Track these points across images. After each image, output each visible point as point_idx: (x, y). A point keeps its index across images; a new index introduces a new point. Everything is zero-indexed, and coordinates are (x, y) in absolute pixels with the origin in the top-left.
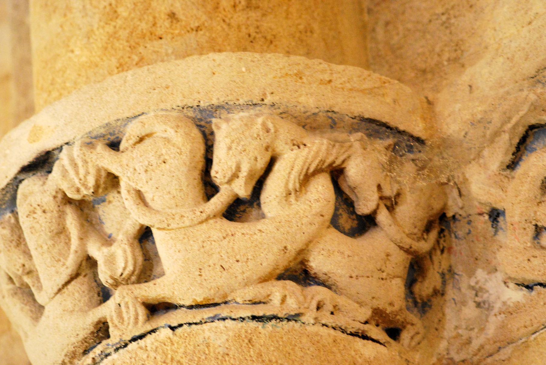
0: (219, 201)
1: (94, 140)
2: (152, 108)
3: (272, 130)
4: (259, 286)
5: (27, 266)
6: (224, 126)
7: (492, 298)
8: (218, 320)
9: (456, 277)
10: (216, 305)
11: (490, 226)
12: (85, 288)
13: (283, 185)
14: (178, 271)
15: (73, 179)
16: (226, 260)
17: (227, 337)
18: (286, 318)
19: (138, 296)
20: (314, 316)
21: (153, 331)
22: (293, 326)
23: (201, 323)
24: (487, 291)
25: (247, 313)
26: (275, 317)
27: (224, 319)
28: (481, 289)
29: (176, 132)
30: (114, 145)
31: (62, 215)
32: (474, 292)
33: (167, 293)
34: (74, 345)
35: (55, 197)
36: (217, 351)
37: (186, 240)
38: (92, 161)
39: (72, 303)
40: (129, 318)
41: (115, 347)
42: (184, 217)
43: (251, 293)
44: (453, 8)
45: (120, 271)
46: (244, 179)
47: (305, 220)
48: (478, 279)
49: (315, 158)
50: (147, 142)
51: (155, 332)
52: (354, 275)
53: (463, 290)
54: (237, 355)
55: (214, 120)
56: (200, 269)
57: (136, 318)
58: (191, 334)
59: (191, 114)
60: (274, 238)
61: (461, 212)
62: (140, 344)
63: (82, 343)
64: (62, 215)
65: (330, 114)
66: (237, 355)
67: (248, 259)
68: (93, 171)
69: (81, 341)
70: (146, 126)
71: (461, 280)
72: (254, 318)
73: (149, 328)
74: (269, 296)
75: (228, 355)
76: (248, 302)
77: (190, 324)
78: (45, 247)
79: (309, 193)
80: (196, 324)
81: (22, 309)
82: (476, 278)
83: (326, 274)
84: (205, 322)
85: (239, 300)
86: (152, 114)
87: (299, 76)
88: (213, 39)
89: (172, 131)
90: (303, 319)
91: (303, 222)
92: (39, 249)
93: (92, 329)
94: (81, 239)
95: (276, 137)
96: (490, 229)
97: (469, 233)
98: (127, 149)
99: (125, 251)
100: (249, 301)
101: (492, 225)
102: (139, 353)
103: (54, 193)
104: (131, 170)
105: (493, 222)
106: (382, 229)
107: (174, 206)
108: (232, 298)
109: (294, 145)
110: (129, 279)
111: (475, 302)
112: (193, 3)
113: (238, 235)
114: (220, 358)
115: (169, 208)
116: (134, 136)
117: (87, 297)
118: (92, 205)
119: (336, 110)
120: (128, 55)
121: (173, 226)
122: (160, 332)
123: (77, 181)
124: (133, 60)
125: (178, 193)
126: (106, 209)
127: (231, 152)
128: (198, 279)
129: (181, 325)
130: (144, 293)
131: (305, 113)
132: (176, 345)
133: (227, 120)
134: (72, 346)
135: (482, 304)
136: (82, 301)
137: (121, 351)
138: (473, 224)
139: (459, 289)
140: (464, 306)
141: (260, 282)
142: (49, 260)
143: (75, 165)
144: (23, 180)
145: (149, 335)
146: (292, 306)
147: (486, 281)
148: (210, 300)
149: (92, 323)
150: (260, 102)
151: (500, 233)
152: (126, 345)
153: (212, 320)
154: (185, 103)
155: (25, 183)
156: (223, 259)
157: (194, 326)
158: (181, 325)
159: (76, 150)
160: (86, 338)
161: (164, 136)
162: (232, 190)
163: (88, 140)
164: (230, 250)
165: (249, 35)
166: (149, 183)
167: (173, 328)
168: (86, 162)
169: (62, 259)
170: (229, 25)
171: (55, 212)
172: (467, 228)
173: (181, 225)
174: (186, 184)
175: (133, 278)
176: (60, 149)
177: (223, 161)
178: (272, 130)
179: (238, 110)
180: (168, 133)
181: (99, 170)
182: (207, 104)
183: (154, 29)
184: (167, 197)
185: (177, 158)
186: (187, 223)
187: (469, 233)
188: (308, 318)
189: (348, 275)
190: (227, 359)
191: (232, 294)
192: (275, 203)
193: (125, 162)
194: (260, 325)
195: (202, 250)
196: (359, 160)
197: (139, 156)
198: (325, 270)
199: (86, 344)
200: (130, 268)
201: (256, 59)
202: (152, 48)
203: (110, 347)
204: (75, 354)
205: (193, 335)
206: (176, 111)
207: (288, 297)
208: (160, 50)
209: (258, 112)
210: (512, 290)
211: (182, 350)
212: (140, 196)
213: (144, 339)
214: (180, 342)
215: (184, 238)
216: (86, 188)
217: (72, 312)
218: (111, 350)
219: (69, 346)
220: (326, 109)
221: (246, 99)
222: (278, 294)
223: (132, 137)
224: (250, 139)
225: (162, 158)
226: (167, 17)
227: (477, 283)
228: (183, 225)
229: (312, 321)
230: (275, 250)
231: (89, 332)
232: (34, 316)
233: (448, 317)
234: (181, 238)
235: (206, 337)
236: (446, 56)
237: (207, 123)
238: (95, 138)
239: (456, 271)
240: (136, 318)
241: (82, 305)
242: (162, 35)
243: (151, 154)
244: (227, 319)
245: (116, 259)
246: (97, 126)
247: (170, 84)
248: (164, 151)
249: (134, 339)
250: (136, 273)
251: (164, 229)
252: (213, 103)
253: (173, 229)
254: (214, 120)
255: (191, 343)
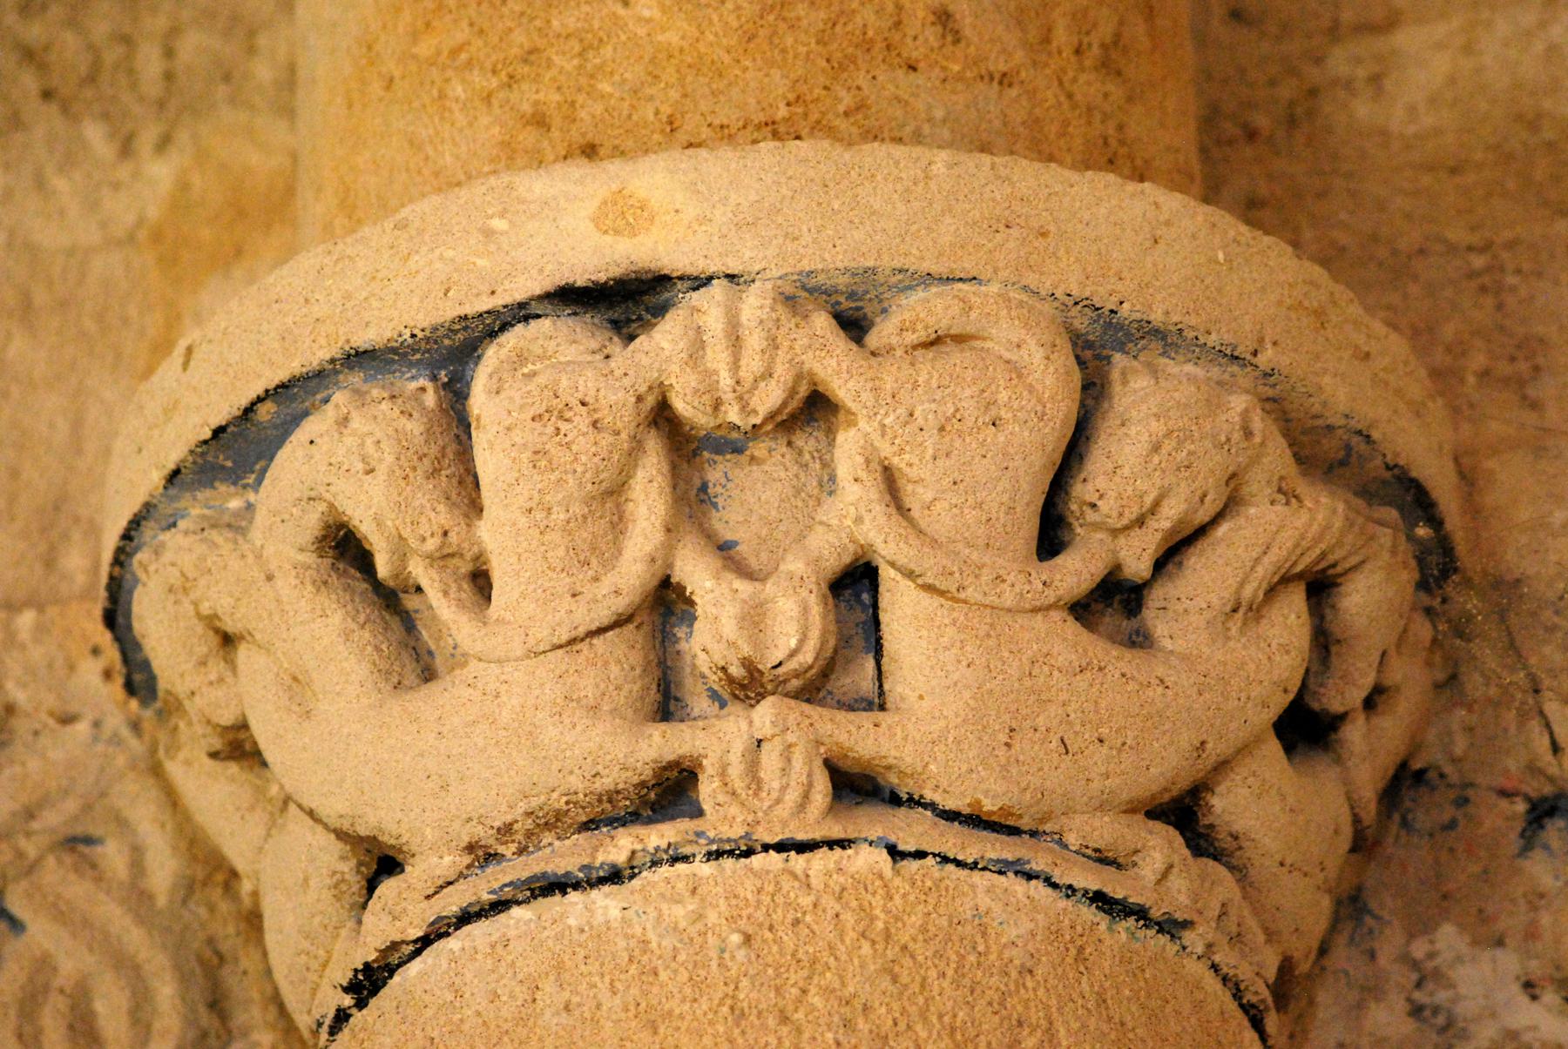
0: (1076, 570)
1: (805, 294)
2: (1003, 274)
3: (1257, 440)
4: (1124, 818)
5: (453, 538)
6: (1141, 382)
7: (1465, 1009)
8: (1016, 873)
9: (1369, 920)
10: (1014, 831)
11: (1519, 829)
12: (636, 658)
13: (1233, 582)
14: (957, 716)
15: (716, 372)
16: (1078, 728)
17: (1032, 925)
18: (1158, 923)
19: (827, 740)
20: (1210, 937)
21: (843, 844)
22: (1164, 948)
23: (974, 866)
24: (1453, 986)
25: (1088, 878)
26: (1141, 913)
27: (1030, 876)
28: (1437, 974)
29: (1048, 358)
30: (854, 326)
31: (636, 449)
32: (1415, 976)
33: (908, 760)
34: (574, 798)
35: (639, 399)
36: (1006, 955)
37: (992, 642)
38: (791, 348)
39: (597, 686)
40: (784, 789)
41: (714, 847)
42: (1004, 581)
43: (1106, 831)
44: (1511, 245)
45: (778, 655)
46: (1159, 536)
47: (1256, 691)
48: (1438, 946)
49: (1317, 540)
50: (956, 357)
51: (844, 848)
52: (1288, 861)
53: (1383, 961)
54: (1052, 982)
55: (1118, 357)
56: (1012, 730)
57: (806, 796)
58: (943, 886)
59: (1081, 323)
60: (1189, 710)
61: (1448, 769)
62: (792, 863)
63: (600, 801)
64: (636, 449)
65: (1356, 440)
66: (1052, 982)
67: (1124, 744)
68: (783, 372)
69: (601, 795)
70: (973, 315)
71: (1381, 933)
72: (1100, 899)
73: (837, 832)
74: (1136, 852)
75: (1030, 972)
76: (1089, 852)
77: (945, 860)
78: (559, 516)
79: (1264, 621)
80: (959, 864)
81: (347, 635)
82: (1432, 942)
83: (1236, 838)
84: (984, 869)
85: (1072, 840)
86: (994, 288)
87: (1319, 314)
88: (1037, 120)
89: (1039, 355)
90: (1188, 937)
91: (1253, 694)
92: (539, 515)
93: (647, 774)
94: (669, 530)
95: (1255, 460)
96: (1513, 836)
97: (1452, 825)
98: (890, 349)
99: (805, 610)
100: (1096, 850)
101: (1524, 830)
102: (786, 886)
103: (643, 389)
104: (902, 411)
105: (1530, 823)
106: (1339, 761)
107: (981, 542)
108: (1057, 828)
109: (1280, 490)
110: (785, 682)
111: (1408, 1000)
112: (998, 7)
113: (1113, 672)
114: (1014, 974)
115: (968, 545)
116: (926, 328)
117: (639, 684)
118: (694, 446)
119: (1376, 435)
120: (822, 80)
121: (970, 593)
122: (857, 853)
123: (725, 381)
124: (839, 100)
125: (1002, 515)
126: (738, 475)
127: (1156, 459)
128: (1001, 751)
129: (920, 855)
130: (843, 738)
131: (1315, 417)
132: (898, 900)
133: (1154, 372)
134: (565, 799)
135: (1427, 1013)
136: (624, 693)
137: (728, 863)
138: (1471, 809)
139: (1372, 955)
140: (1378, 1000)
141: (1125, 812)
142: (561, 552)
143: (735, 342)
144: (538, 316)
145: (825, 849)
146: (1178, 897)
147: (1459, 959)
148: (1013, 815)
149: (655, 761)
150: (1249, 357)
151: (1538, 854)
152: (748, 853)
153: (1001, 868)
154: (1087, 294)
155: (545, 324)
156: (1070, 723)
157: (951, 867)
158: (920, 855)
159: (754, 305)
160: (618, 792)
161: (1007, 355)
162: (1114, 552)
163: (789, 289)
164: (1089, 706)
165: (1106, 143)
166: (940, 462)
167: (894, 853)
168: (774, 344)
169: (594, 562)
170: (1070, 96)
171: (624, 436)
172: (1448, 813)
173: (992, 599)
174: (1027, 498)
175: (795, 683)
176: (700, 282)
177: (1126, 471)
178: (1257, 440)
179: (1190, 356)
180: (1024, 352)
181: (799, 377)
182: (1138, 316)
183: (897, 37)
184: (971, 515)
185: (1030, 424)
186: (1009, 599)
187: (1452, 825)
188: (1194, 940)
189: (1278, 857)
190: (1030, 984)
191: (1064, 819)
192: (1196, 620)
193: (889, 385)
194: (1103, 920)
195: (1028, 683)
196: (1379, 576)
197: (934, 383)
198: (1237, 827)
199: (608, 806)
200: (807, 657)
201: (1243, 240)
202: (891, 87)
203: (702, 841)
204: (558, 820)
205: (947, 889)
206: (1056, 304)
207: (1175, 870)
208: (911, 100)
209: (1226, 376)
210: (1549, 1010)
211: (915, 920)
212: (890, 481)
213: (807, 855)
214: (912, 898)
215: (988, 636)
216: (745, 409)
217: (594, 708)
218: (700, 850)
219: (555, 795)
220: (1359, 427)
221: (1228, 338)
222: (1157, 855)
223: (919, 326)
224: (1208, 444)
225: (993, 412)
226: (932, 18)
227: (1431, 956)
228: (997, 602)
229: (1200, 950)
230: (1185, 744)
231: (636, 780)
232: (383, 665)
233: (1321, 1014)
234: (982, 633)
235: (982, 909)
236: (1478, 360)
237: (1097, 357)
238: (810, 291)
239: (1373, 905)
240: (806, 796)
241: (622, 700)
242: (918, 61)
243: (968, 392)
244: (1037, 877)
245: (756, 614)
246: (840, 265)
247: (1052, 228)
248: (1003, 396)
249: (781, 847)
250: (808, 675)
251: (942, 593)
252: (1151, 318)
253: (965, 602)
254: (1118, 357)
255: (942, 910)
